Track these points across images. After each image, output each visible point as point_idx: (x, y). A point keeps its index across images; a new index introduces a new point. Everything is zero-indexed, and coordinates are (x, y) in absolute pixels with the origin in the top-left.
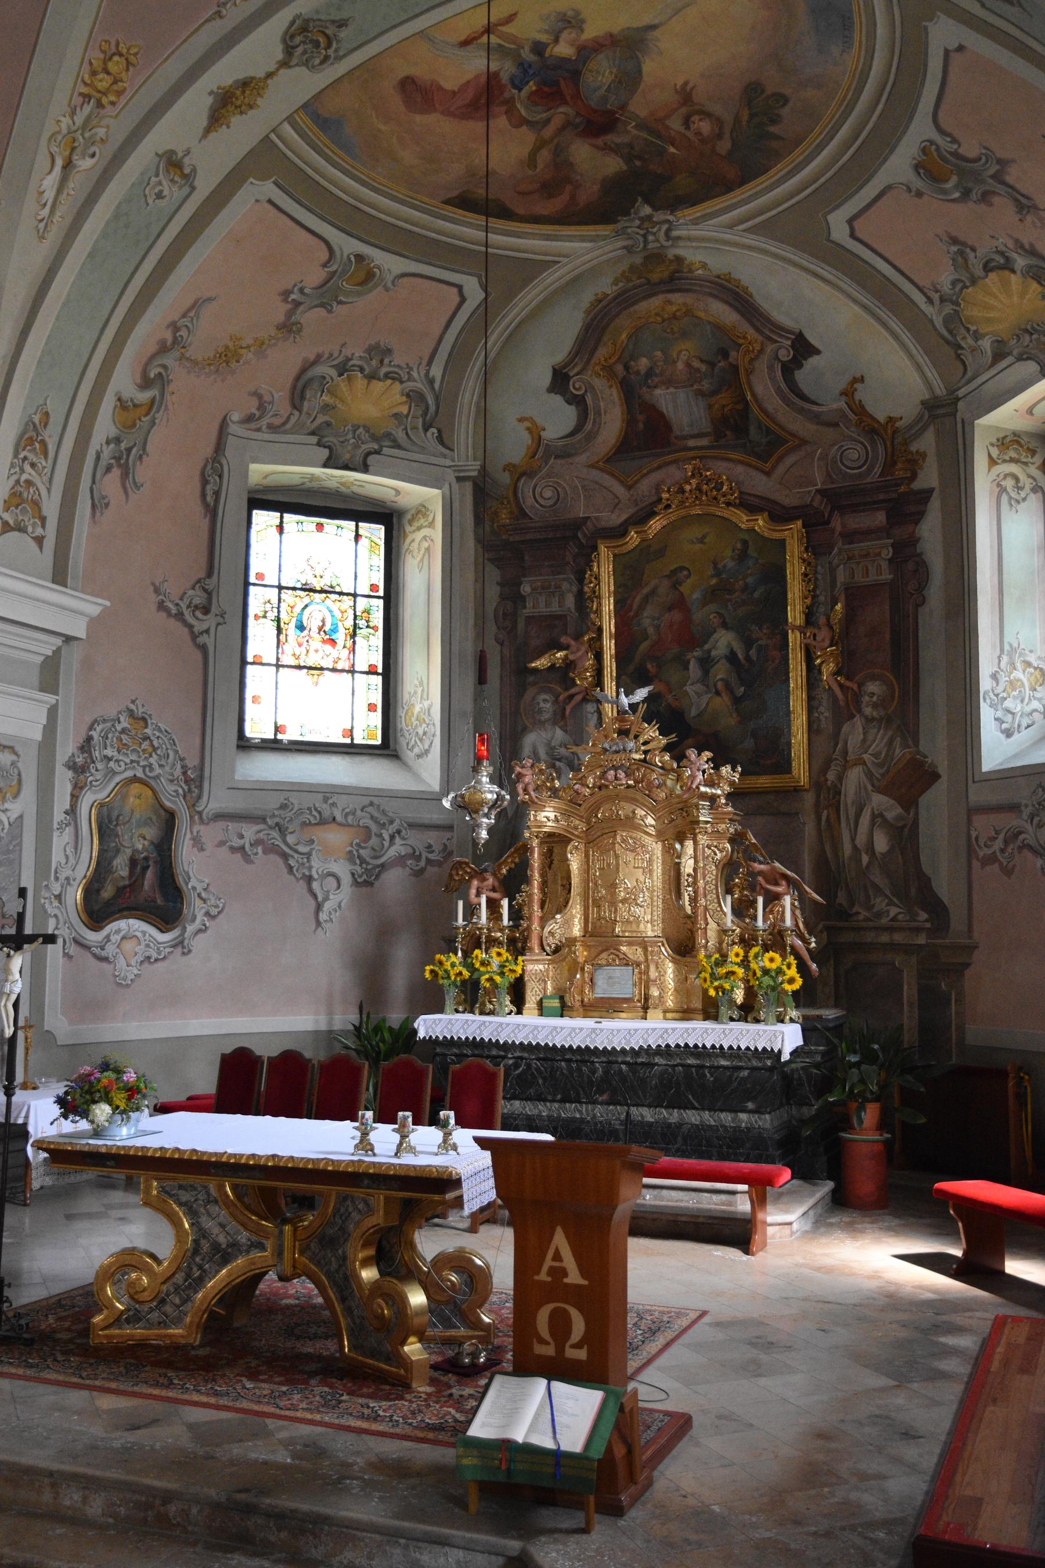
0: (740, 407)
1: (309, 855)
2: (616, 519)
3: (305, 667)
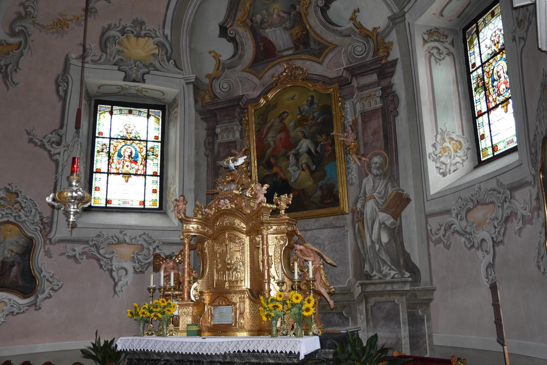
0: (304, 33)
1: (111, 259)
3: (121, 174)
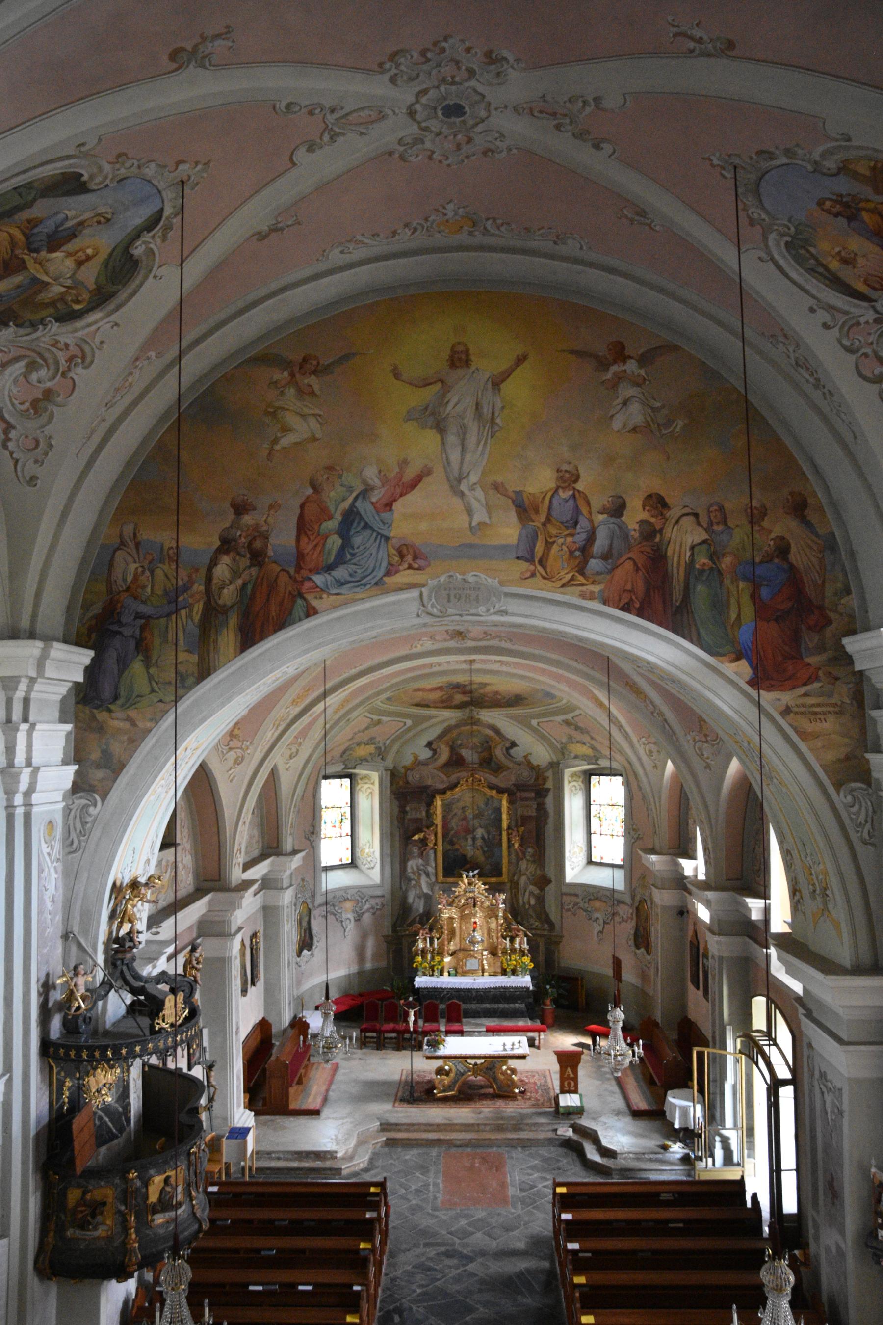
2: (442, 786)
